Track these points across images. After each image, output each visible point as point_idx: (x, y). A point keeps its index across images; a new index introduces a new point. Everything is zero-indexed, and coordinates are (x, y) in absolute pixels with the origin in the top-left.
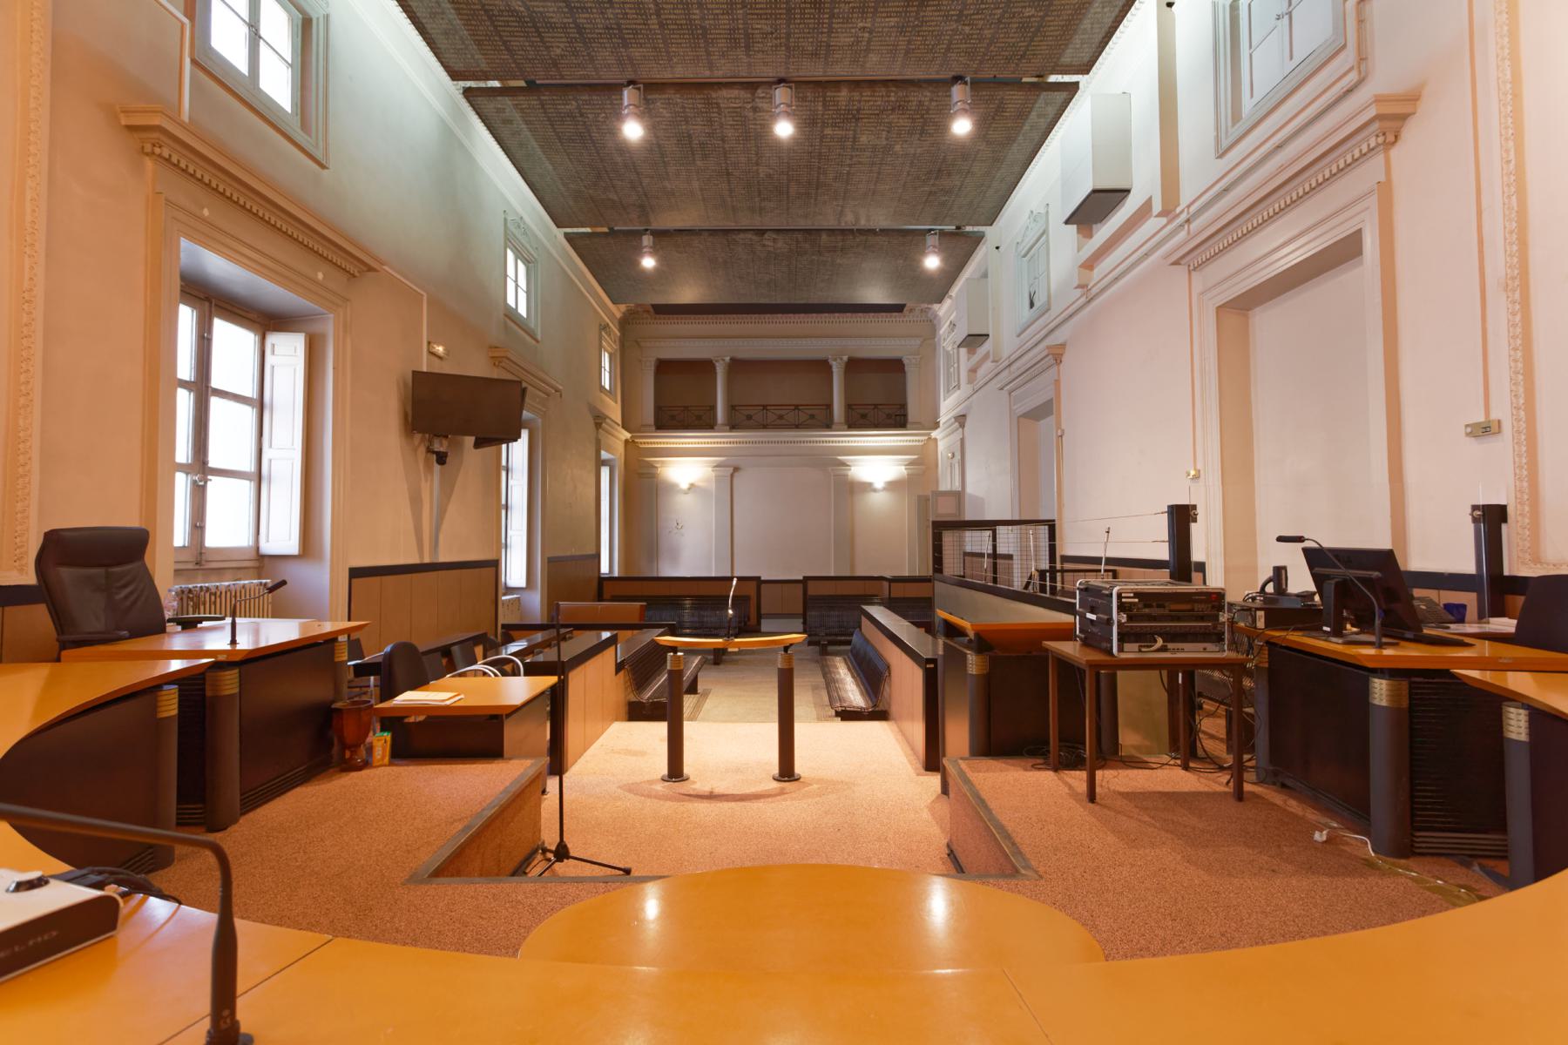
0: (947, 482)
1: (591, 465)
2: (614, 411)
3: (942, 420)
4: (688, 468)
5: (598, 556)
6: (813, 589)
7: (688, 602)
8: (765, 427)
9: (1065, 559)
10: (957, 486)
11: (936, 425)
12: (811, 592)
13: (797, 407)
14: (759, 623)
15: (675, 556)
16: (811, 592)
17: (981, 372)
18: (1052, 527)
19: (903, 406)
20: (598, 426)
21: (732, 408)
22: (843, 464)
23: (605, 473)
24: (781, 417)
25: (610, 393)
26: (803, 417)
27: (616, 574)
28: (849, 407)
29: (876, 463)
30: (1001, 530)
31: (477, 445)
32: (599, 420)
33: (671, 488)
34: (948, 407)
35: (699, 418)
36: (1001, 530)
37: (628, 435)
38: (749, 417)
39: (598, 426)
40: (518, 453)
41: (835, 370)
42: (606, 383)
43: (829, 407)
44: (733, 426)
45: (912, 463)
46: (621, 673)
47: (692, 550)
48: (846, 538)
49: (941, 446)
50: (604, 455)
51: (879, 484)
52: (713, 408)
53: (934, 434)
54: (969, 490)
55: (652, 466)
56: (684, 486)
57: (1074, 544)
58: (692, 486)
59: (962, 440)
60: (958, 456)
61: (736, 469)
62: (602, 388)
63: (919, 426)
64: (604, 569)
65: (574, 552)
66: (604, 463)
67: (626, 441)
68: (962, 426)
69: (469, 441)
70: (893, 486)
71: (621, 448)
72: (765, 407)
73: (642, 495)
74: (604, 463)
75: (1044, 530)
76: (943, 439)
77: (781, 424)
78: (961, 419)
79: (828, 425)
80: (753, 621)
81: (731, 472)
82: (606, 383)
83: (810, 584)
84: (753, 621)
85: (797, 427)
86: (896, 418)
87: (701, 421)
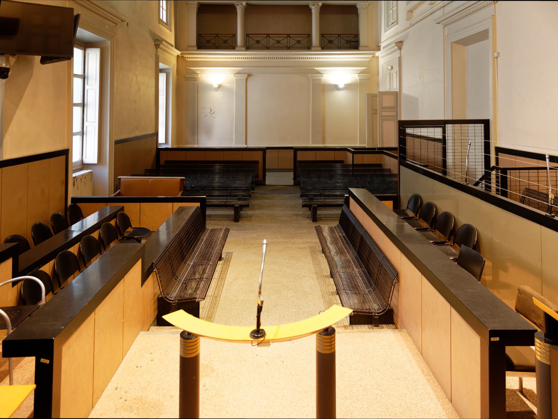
0: (387, 84)
1: (152, 73)
2: (170, 36)
3: (382, 45)
4: (219, 73)
5: (156, 134)
6: (301, 156)
7: (217, 167)
8: (268, 48)
9: (499, 150)
10: (395, 87)
11: (378, 48)
12: (299, 158)
13: (288, 35)
14: (264, 179)
15: (209, 132)
16: (299, 158)
17: (416, 13)
18: (486, 123)
19: (357, 36)
20: (157, 46)
21: (247, 36)
22: (318, 72)
23: (162, 77)
24: (278, 42)
25: (167, 24)
26: (292, 42)
27: (169, 146)
28: (322, 36)
29: (339, 71)
30: (449, 127)
31: (43, 61)
32: (158, 42)
33: (208, 87)
34: (387, 36)
35: (225, 42)
36: (449, 127)
37: (179, 53)
38: (258, 42)
39: (157, 46)
40: (86, 63)
41: (313, 11)
42: (164, 18)
43: (309, 36)
44: (248, 47)
45: (362, 72)
46: (150, 280)
47: (220, 132)
48: (319, 122)
49: (382, 62)
50: (161, 66)
51: (341, 86)
52: (235, 36)
53: (378, 54)
54: (405, 91)
55: (194, 73)
56: (216, 86)
57: (502, 139)
58: (220, 86)
59: (400, 58)
60: (396, 68)
61: (249, 75)
62: (160, 21)
63: (367, 48)
64: (161, 139)
65: (138, 134)
66: (162, 71)
67: (178, 56)
68: (400, 48)
69: (38, 58)
70: (349, 87)
71: (174, 61)
72: (268, 35)
73: (186, 92)
74: (162, 71)
75: (481, 127)
76: (383, 58)
77: (278, 46)
78: (400, 44)
79: (309, 47)
80: (261, 178)
81: (247, 76)
82: (164, 18)
83: (299, 153)
84: (261, 178)
85: (289, 48)
86: (352, 43)
87: (227, 44)
